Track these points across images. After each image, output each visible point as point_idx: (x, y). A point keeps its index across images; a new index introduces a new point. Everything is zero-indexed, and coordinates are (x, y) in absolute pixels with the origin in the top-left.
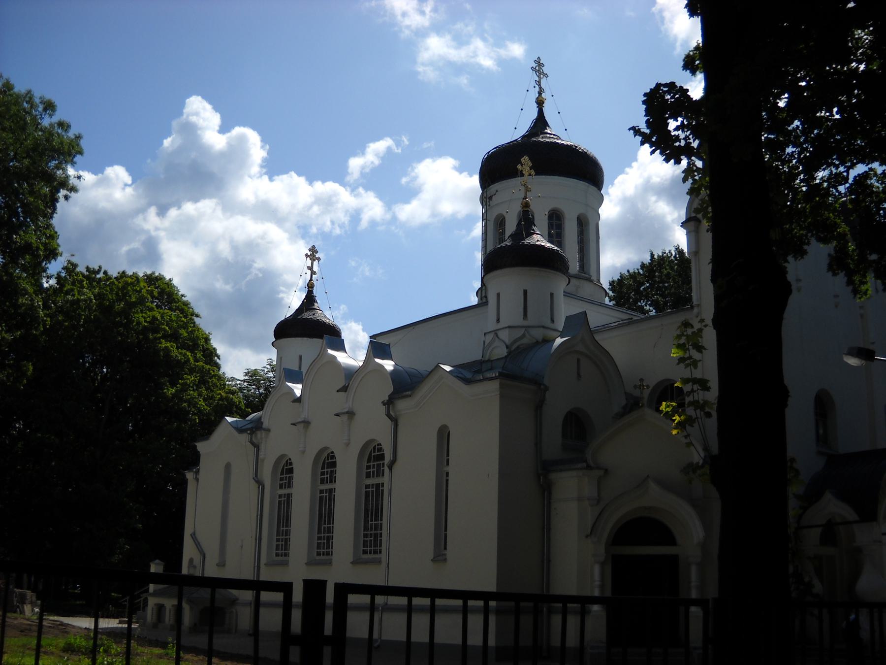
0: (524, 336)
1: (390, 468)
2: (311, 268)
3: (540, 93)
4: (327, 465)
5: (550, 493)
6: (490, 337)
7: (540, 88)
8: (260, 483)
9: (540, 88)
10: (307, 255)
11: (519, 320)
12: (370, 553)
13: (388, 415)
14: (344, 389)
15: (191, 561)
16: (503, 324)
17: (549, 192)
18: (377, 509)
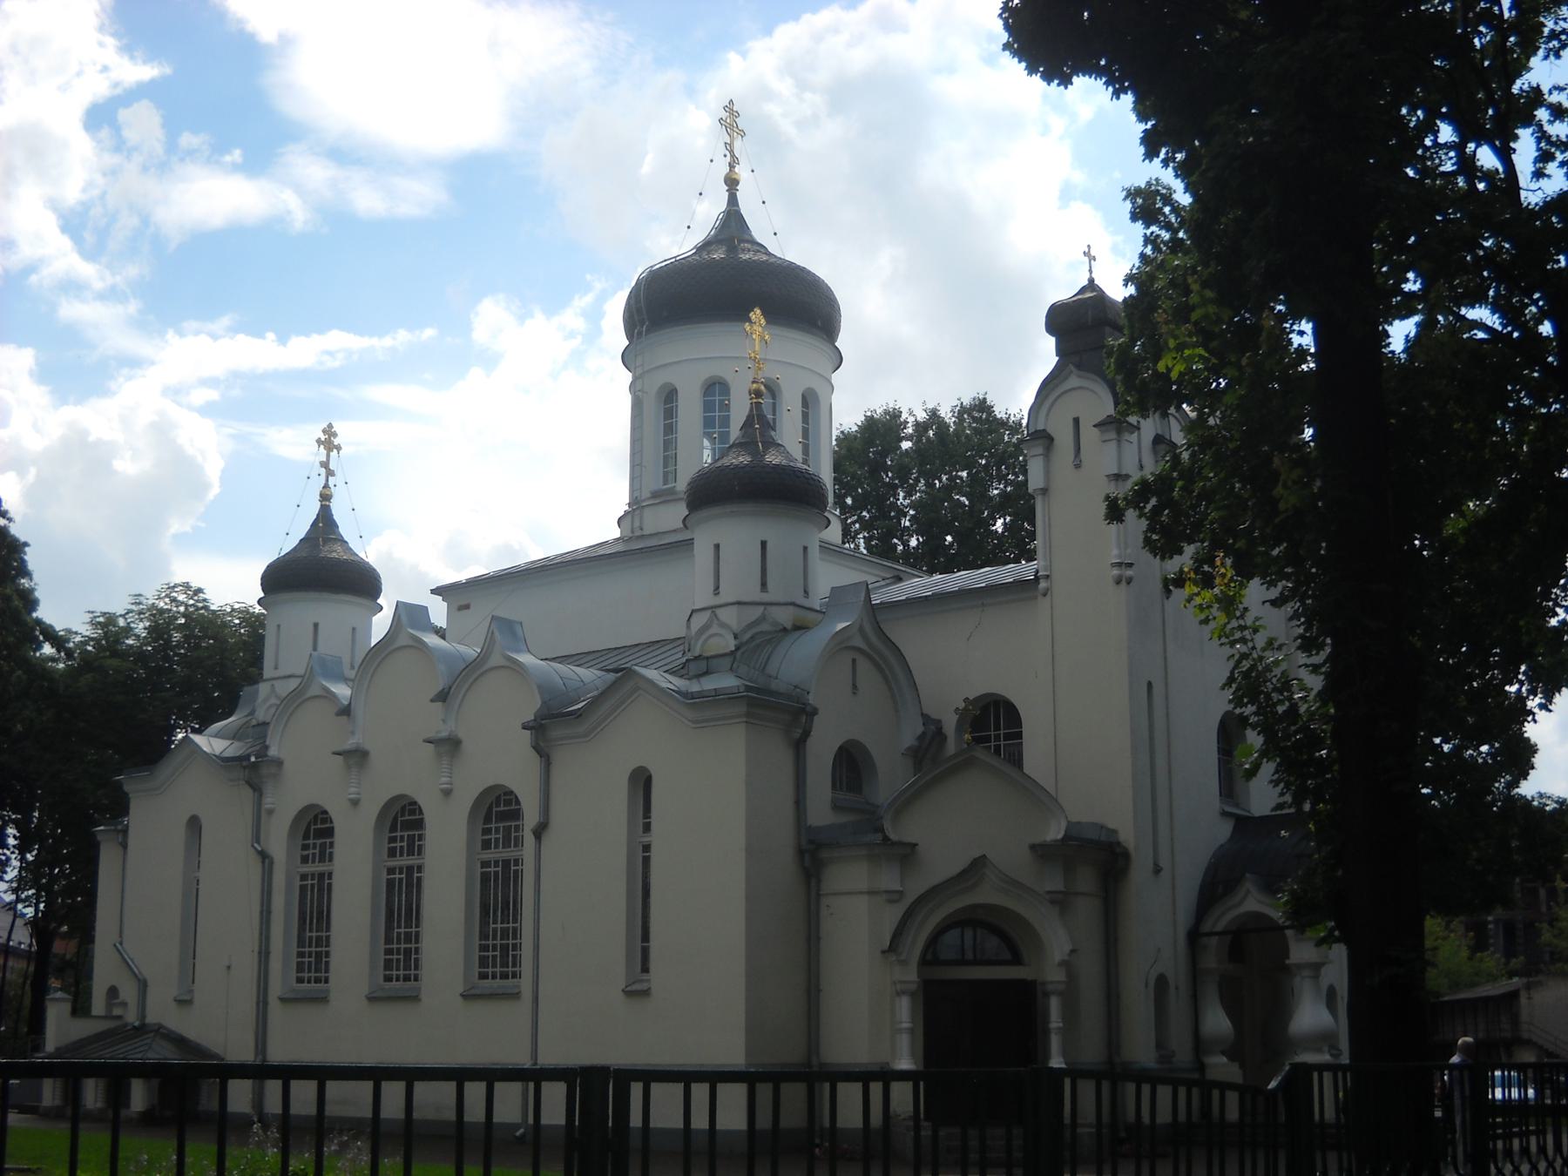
0: (762, 619)
1: (539, 832)
2: (325, 465)
3: (732, 166)
4: (403, 822)
5: (819, 881)
6: (699, 621)
7: (733, 156)
8: (264, 856)
9: (733, 156)
10: (319, 442)
11: (755, 594)
12: (494, 977)
13: (537, 748)
14: (443, 696)
15: (113, 992)
16: (727, 595)
17: (753, 347)
18: (320, 913)
